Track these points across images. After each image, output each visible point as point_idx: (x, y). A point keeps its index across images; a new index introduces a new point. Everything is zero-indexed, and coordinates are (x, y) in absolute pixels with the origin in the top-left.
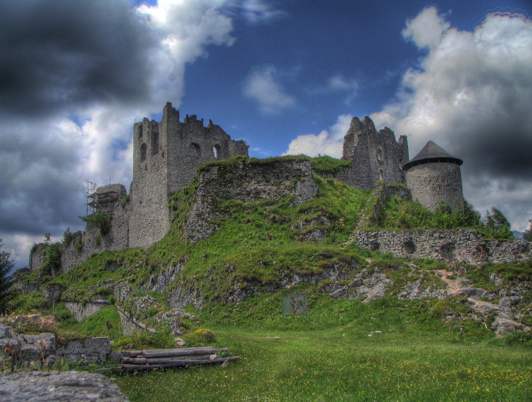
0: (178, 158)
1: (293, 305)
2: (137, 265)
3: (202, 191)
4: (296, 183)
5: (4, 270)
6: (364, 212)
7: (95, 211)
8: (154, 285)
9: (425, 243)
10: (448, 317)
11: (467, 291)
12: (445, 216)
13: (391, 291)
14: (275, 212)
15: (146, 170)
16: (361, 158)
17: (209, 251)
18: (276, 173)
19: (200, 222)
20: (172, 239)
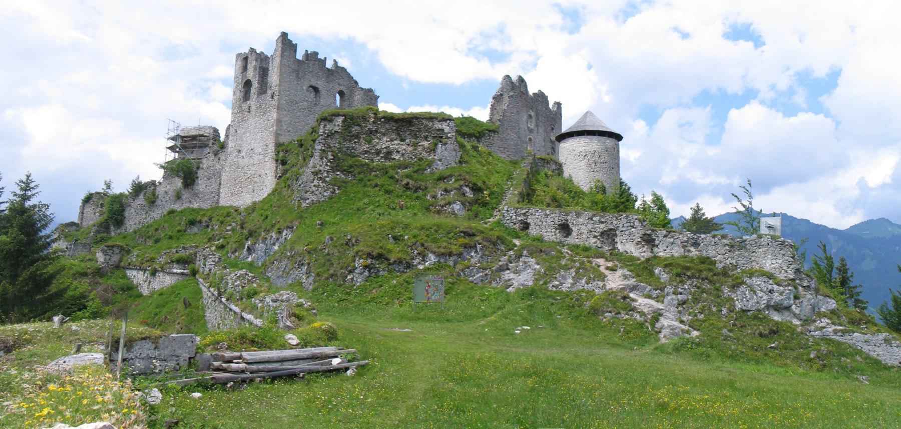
0: (292, 102)
1: (427, 291)
2: (229, 228)
3: (321, 144)
4: (436, 145)
5: (39, 225)
6: (512, 185)
7: (177, 157)
8: (250, 254)
9: (583, 227)
10: (606, 314)
11: (629, 286)
12: (600, 197)
13: (540, 280)
14: (407, 176)
15: (249, 112)
17: (325, 217)
19: (316, 182)
20: (278, 200)
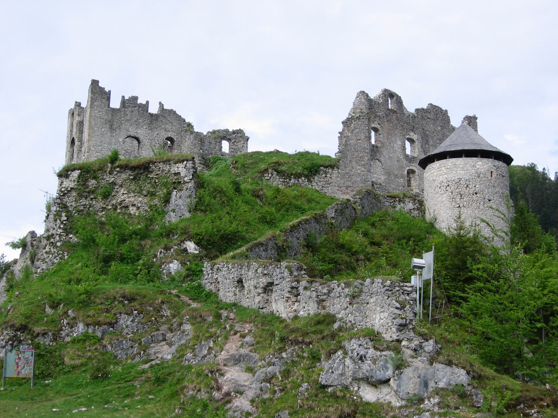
1: (17, 363)
16: (356, 154)
18: (153, 178)
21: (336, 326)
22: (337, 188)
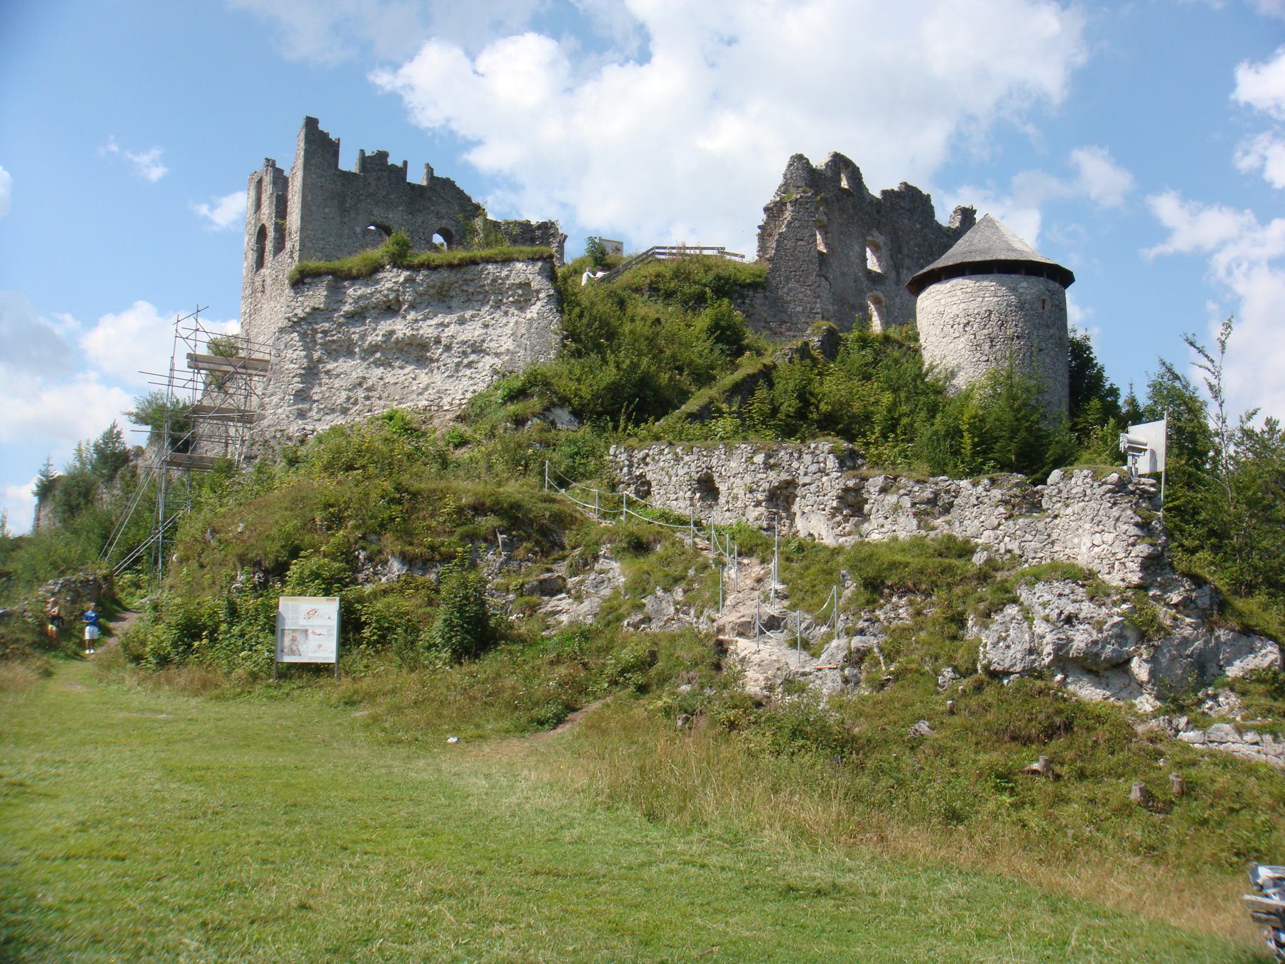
9: (738, 481)
15: (263, 292)
21: (979, 559)
22: (763, 324)
